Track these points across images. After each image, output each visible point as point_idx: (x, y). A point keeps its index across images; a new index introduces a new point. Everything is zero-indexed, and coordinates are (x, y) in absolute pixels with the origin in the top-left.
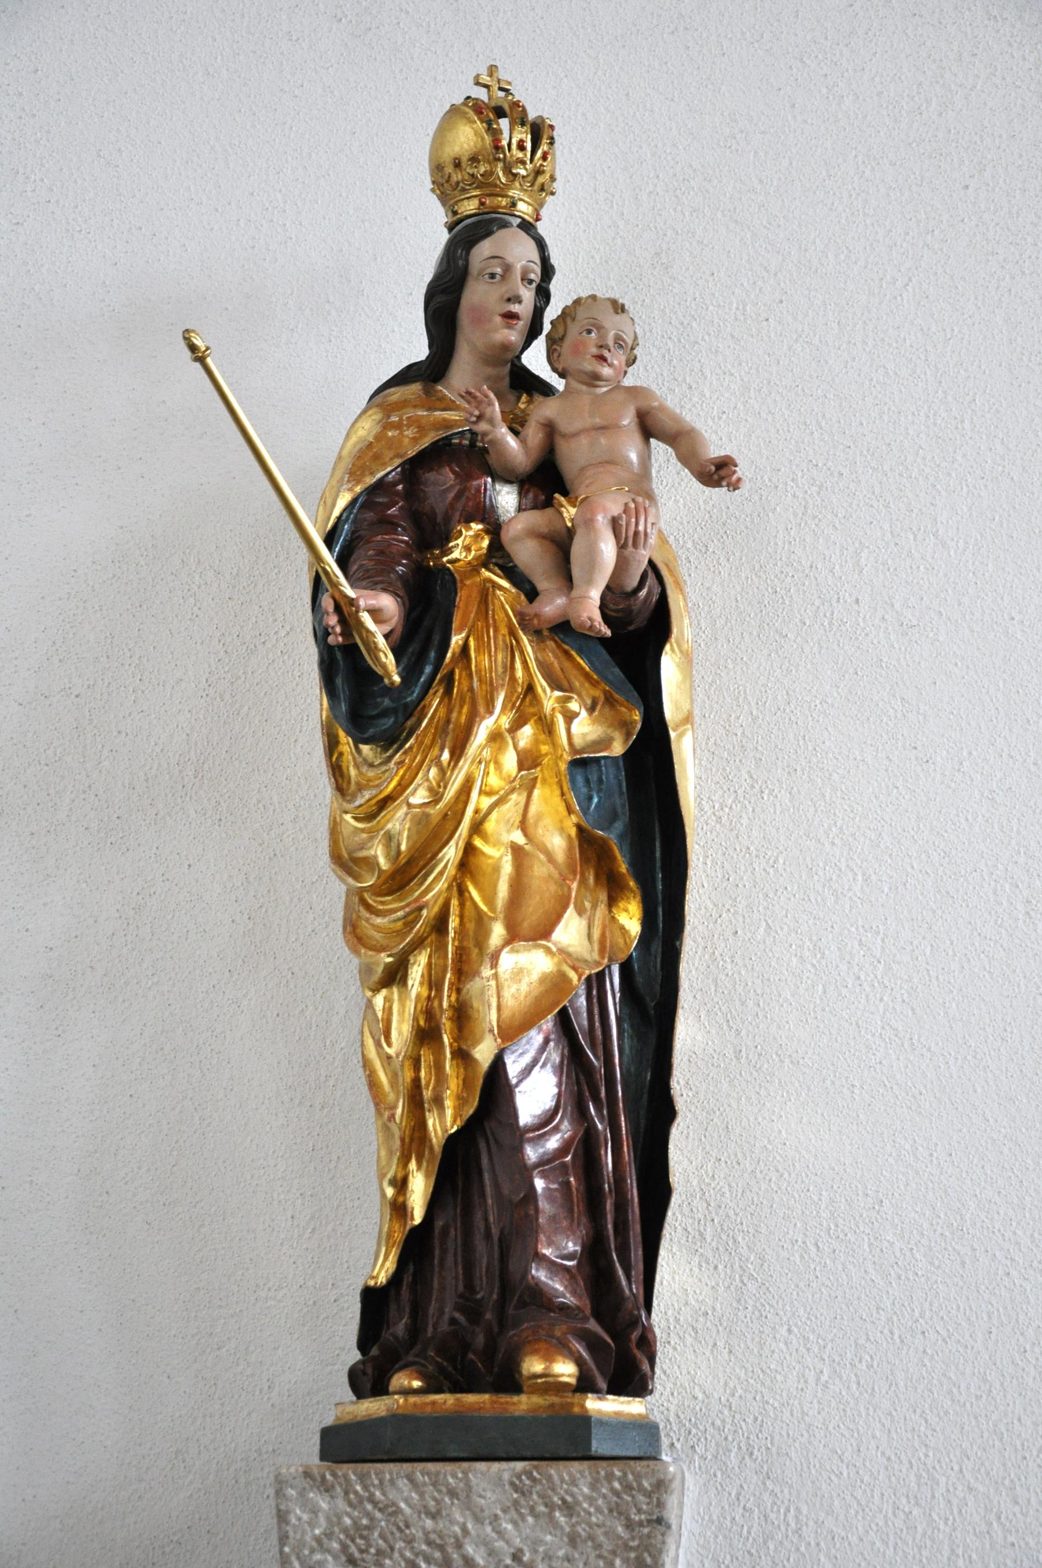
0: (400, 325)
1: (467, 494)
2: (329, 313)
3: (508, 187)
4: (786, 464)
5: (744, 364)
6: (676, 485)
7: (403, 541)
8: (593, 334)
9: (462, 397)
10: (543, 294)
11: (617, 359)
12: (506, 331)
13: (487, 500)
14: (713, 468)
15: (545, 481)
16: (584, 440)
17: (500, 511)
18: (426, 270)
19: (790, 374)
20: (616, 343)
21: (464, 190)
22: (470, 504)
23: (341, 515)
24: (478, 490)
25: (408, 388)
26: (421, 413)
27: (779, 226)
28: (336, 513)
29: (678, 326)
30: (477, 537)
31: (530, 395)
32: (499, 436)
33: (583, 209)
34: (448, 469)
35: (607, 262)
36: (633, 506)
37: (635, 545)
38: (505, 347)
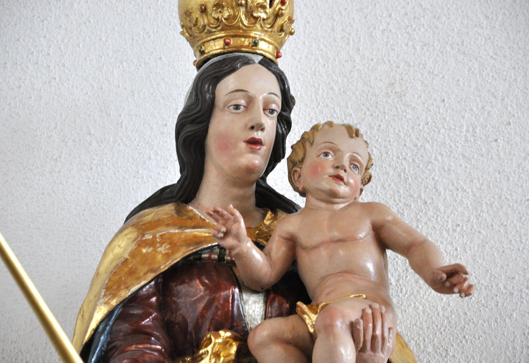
0: (157, 154)
1: (216, 304)
2: (90, 144)
3: (249, 28)
4: (520, 272)
5: (475, 181)
6: (415, 292)
7: (156, 350)
8: (330, 156)
9: (211, 215)
10: (285, 122)
11: (353, 178)
12: (250, 155)
13: (235, 309)
14: (444, 276)
15: (289, 290)
16: (323, 252)
17: (247, 319)
18: (179, 105)
19: (520, 189)
20: (351, 164)
21: (210, 32)
22: (219, 313)
23: (98, 327)
24: (226, 300)
25: (161, 208)
26: (173, 231)
27: (505, 56)
28: (93, 325)
29: (412, 147)
30: (226, 344)
31: (274, 212)
32: (245, 250)
33: (322, 47)
34: (198, 281)
35: (345, 92)
36: (369, 311)
37: (373, 348)
38: (250, 170)
